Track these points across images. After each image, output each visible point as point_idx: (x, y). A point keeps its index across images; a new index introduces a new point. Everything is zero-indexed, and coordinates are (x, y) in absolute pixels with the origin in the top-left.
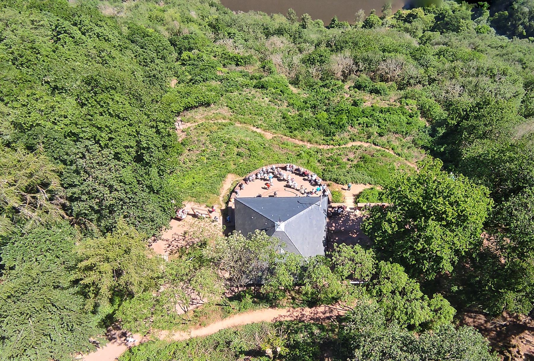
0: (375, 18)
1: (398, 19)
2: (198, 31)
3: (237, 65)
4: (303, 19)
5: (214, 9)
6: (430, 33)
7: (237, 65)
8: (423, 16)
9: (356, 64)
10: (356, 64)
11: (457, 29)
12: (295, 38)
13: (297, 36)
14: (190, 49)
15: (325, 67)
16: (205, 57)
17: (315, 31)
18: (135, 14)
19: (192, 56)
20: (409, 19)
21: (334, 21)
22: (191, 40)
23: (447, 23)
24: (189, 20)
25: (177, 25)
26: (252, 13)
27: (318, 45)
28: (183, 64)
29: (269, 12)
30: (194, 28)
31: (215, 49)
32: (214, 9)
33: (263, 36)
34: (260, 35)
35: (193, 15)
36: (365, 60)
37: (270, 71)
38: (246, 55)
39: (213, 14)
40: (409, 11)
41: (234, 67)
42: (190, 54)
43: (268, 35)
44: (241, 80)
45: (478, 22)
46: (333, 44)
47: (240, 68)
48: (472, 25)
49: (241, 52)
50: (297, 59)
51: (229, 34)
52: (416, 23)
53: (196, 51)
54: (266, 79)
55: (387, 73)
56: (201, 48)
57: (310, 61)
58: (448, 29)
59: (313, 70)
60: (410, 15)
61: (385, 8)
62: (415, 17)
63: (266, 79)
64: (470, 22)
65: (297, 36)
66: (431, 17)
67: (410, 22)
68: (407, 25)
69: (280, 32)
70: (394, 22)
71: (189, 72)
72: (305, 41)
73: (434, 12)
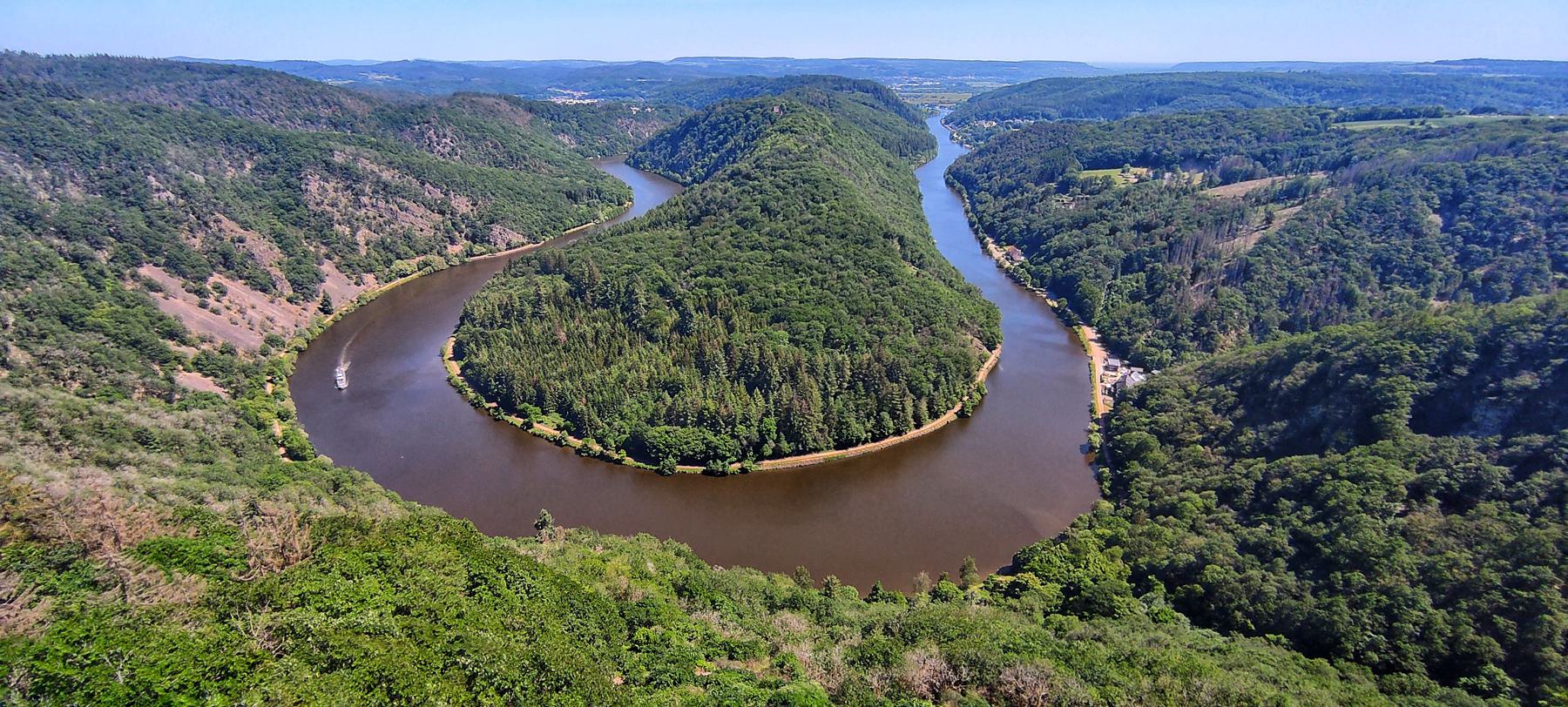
0: (949, 586)
1: (992, 591)
2: (657, 595)
3: (731, 658)
4: (827, 585)
5: (682, 560)
6: (1060, 617)
7: (731, 658)
8: (1038, 587)
9: (955, 669)
10: (955, 669)
11: (1110, 613)
12: (819, 617)
13: (823, 612)
14: (649, 624)
15: (895, 673)
16: (675, 641)
17: (848, 603)
18: (558, 562)
19: (652, 636)
20: (1014, 591)
21: (875, 589)
22: (653, 611)
23: (1088, 601)
24: (645, 576)
25: (623, 582)
26: (737, 570)
27: (867, 631)
28: (634, 649)
29: (766, 568)
30: (652, 588)
31: (690, 626)
32: (682, 560)
33: (765, 611)
34: (758, 607)
35: (651, 567)
36: (972, 664)
37: (793, 675)
38: (746, 640)
39: (681, 569)
40: (1010, 579)
41: (725, 661)
42: (650, 631)
43: (773, 608)
44: (744, 688)
45: (1149, 602)
46: (896, 630)
47: (737, 665)
48: (1140, 607)
49: (734, 634)
50: (837, 654)
51: (713, 602)
52: (1027, 599)
53: (659, 627)
54: (790, 688)
55: (1018, 691)
56: (667, 623)
57: (864, 659)
58: (1092, 612)
59: (873, 677)
60: (1014, 585)
61: (963, 571)
62: (1024, 587)
63: (790, 688)
64: (1135, 602)
65: (823, 612)
66: (1053, 589)
67: (1018, 597)
68: (1011, 601)
69: (793, 604)
70: (987, 595)
71: (647, 665)
72: (840, 622)
73: (1058, 581)
